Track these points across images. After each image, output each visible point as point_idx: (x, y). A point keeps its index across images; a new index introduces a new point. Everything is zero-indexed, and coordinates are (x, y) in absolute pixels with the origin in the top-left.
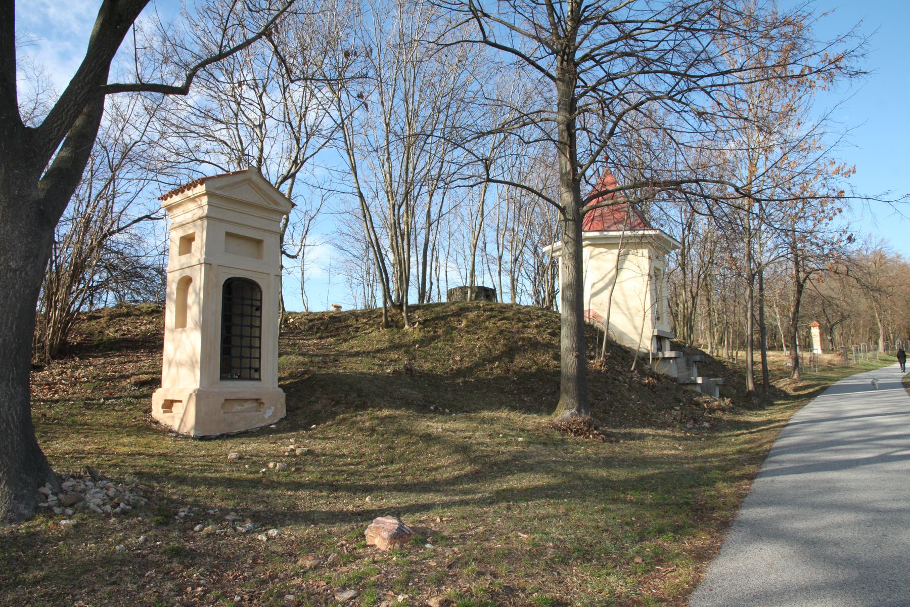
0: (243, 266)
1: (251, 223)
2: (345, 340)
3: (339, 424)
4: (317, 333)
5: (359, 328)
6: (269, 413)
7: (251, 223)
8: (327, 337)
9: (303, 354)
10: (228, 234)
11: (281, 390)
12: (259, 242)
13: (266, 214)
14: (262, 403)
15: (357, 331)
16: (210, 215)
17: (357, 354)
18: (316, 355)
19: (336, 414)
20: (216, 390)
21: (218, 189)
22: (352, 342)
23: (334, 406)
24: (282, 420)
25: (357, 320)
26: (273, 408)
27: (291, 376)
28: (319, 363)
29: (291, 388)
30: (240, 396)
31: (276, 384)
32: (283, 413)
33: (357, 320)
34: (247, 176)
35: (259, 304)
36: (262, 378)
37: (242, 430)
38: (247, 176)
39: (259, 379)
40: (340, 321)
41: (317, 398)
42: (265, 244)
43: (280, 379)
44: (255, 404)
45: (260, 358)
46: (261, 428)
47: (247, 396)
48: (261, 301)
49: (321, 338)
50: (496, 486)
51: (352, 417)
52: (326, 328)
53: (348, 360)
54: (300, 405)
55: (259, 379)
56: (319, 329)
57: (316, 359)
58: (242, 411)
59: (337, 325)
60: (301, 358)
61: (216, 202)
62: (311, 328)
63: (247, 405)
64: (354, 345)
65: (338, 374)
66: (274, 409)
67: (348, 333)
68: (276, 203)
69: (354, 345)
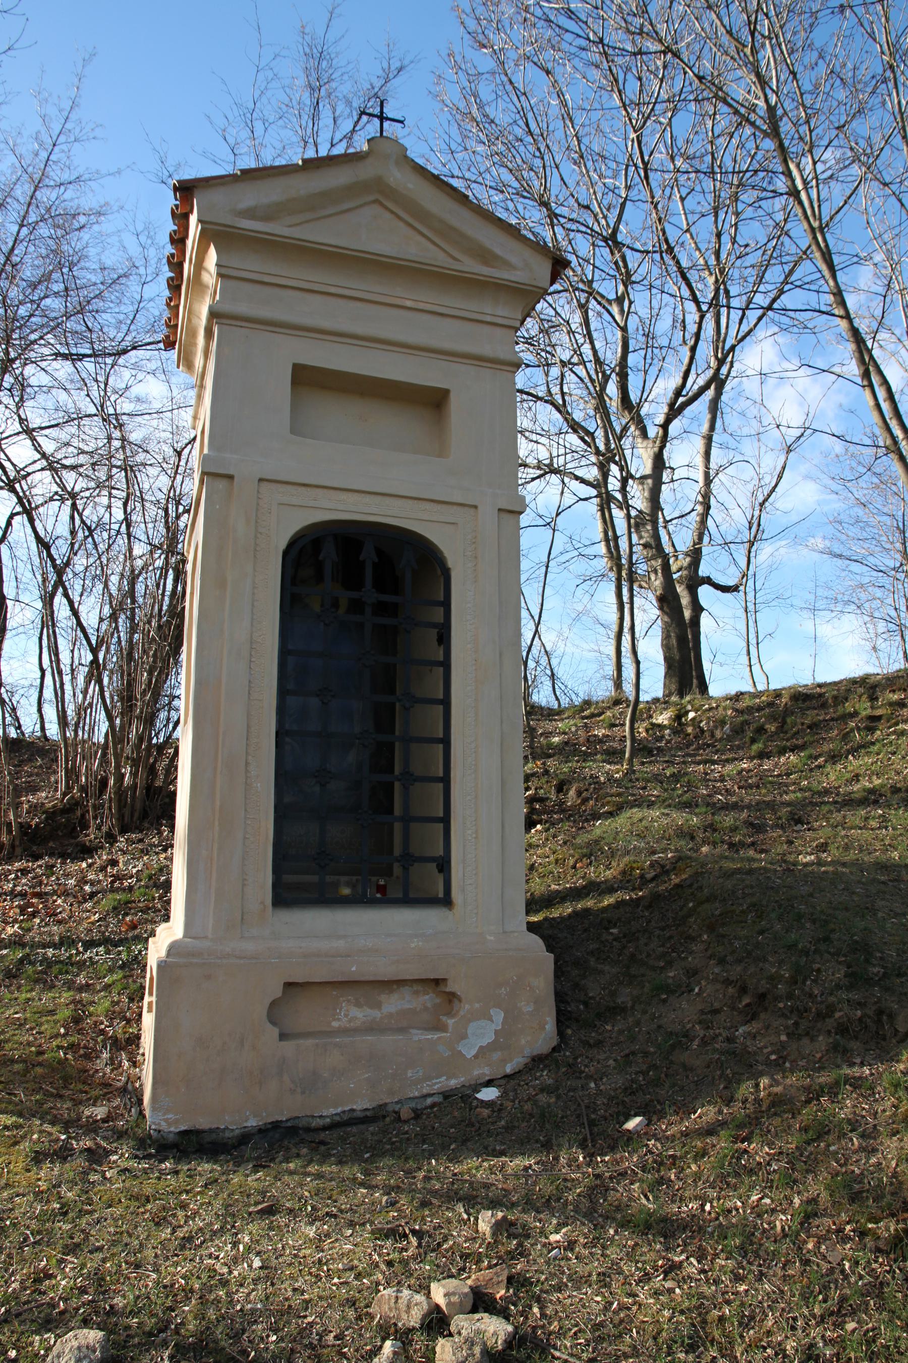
0: (367, 478)
1: (393, 334)
2: (834, 758)
3: (748, 1127)
4: (753, 741)
5: (879, 718)
6: (481, 1034)
7: (393, 334)
8: (782, 751)
9: (688, 805)
10: (305, 378)
11: (536, 941)
12: (434, 401)
13: (453, 302)
14: (452, 997)
15: (871, 730)
16: (228, 308)
17: (872, 798)
18: (735, 807)
19: (746, 1064)
20: (249, 947)
21: (249, 213)
22: (854, 763)
23: (750, 1015)
24: (537, 1061)
25: (873, 698)
26: (498, 1016)
27: (626, 880)
28: (734, 829)
29: (611, 923)
30: (353, 970)
31: (520, 919)
32: (541, 1033)
33: (873, 698)
34: (364, 172)
35: (438, 615)
36: (456, 894)
37: (361, 1104)
38: (364, 172)
39: (446, 901)
40: (824, 706)
41: (692, 973)
42: (455, 404)
43: (532, 905)
44: (428, 999)
45: (446, 820)
46: (447, 1095)
47: (385, 969)
48: (446, 604)
49: (763, 755)
50: (486, 270)
51: (813, 1094)
52: (781, 729)
53: (837, 817)
54: (624, 997)
55: (446, 901)
56: (761, 730)
57: (728, 820)
58: (371, 1028)
59: (812, 716)
60: (680, 818)
61: (250, 263)
62: (738, 731)
63: (394, 1003)
64: (863, 770)
65: (790, 869)
66: (498, 1028)
67: (846, 737)
68: (486, 256)
69: (863, 770)
